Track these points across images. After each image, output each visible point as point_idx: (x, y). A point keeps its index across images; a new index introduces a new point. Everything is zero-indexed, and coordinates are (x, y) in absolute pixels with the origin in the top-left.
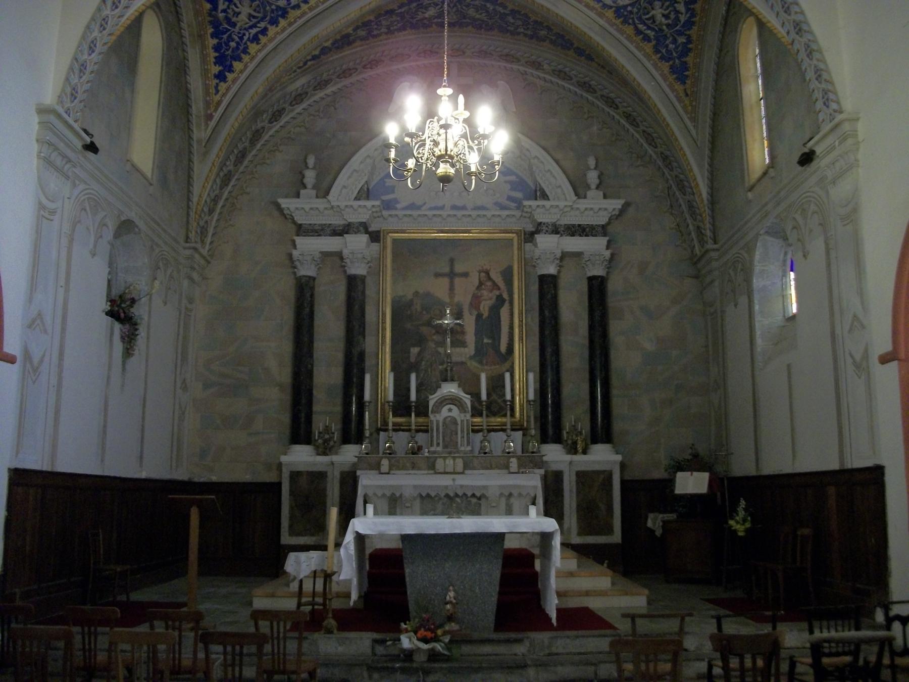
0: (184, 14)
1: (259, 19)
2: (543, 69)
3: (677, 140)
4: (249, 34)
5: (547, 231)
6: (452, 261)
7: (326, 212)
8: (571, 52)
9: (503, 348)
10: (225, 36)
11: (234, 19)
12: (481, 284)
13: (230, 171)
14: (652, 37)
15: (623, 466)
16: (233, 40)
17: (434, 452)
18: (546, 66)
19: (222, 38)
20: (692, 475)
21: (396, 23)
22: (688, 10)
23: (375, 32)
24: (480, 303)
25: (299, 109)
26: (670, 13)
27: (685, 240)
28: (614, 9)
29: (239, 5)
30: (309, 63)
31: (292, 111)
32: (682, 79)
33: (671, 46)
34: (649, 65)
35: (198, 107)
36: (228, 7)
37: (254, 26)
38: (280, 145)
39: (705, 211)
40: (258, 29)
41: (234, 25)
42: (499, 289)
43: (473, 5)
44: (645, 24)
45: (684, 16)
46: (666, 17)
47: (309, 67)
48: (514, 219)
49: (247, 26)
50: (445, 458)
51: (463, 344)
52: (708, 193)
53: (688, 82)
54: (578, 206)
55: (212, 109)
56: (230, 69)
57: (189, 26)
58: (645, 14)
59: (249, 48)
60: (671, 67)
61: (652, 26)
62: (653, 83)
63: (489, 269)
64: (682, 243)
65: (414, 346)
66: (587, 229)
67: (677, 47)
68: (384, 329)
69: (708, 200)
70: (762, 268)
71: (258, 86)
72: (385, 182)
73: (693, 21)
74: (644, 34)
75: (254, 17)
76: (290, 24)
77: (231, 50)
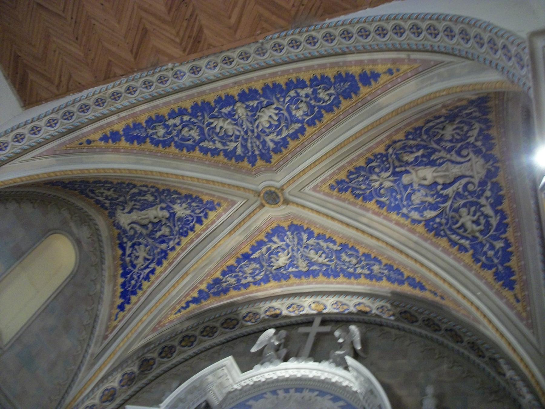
10: (129, 276)
11: (135, 262)
16: (133, 279)
22: (496, 212)
23: (244, 281)
26: (478, 219)
32: (510, 285)
35: (99, 329)
37: (147, 267)
41: (134, 266)
44: (458, 234)
46: (477, 222)
49: (143, 266)
53: (517, 287)
56: (128, 302)
60: (496, 274)
75: (148, 260)
76: (170, 264)
77: (131, 287)
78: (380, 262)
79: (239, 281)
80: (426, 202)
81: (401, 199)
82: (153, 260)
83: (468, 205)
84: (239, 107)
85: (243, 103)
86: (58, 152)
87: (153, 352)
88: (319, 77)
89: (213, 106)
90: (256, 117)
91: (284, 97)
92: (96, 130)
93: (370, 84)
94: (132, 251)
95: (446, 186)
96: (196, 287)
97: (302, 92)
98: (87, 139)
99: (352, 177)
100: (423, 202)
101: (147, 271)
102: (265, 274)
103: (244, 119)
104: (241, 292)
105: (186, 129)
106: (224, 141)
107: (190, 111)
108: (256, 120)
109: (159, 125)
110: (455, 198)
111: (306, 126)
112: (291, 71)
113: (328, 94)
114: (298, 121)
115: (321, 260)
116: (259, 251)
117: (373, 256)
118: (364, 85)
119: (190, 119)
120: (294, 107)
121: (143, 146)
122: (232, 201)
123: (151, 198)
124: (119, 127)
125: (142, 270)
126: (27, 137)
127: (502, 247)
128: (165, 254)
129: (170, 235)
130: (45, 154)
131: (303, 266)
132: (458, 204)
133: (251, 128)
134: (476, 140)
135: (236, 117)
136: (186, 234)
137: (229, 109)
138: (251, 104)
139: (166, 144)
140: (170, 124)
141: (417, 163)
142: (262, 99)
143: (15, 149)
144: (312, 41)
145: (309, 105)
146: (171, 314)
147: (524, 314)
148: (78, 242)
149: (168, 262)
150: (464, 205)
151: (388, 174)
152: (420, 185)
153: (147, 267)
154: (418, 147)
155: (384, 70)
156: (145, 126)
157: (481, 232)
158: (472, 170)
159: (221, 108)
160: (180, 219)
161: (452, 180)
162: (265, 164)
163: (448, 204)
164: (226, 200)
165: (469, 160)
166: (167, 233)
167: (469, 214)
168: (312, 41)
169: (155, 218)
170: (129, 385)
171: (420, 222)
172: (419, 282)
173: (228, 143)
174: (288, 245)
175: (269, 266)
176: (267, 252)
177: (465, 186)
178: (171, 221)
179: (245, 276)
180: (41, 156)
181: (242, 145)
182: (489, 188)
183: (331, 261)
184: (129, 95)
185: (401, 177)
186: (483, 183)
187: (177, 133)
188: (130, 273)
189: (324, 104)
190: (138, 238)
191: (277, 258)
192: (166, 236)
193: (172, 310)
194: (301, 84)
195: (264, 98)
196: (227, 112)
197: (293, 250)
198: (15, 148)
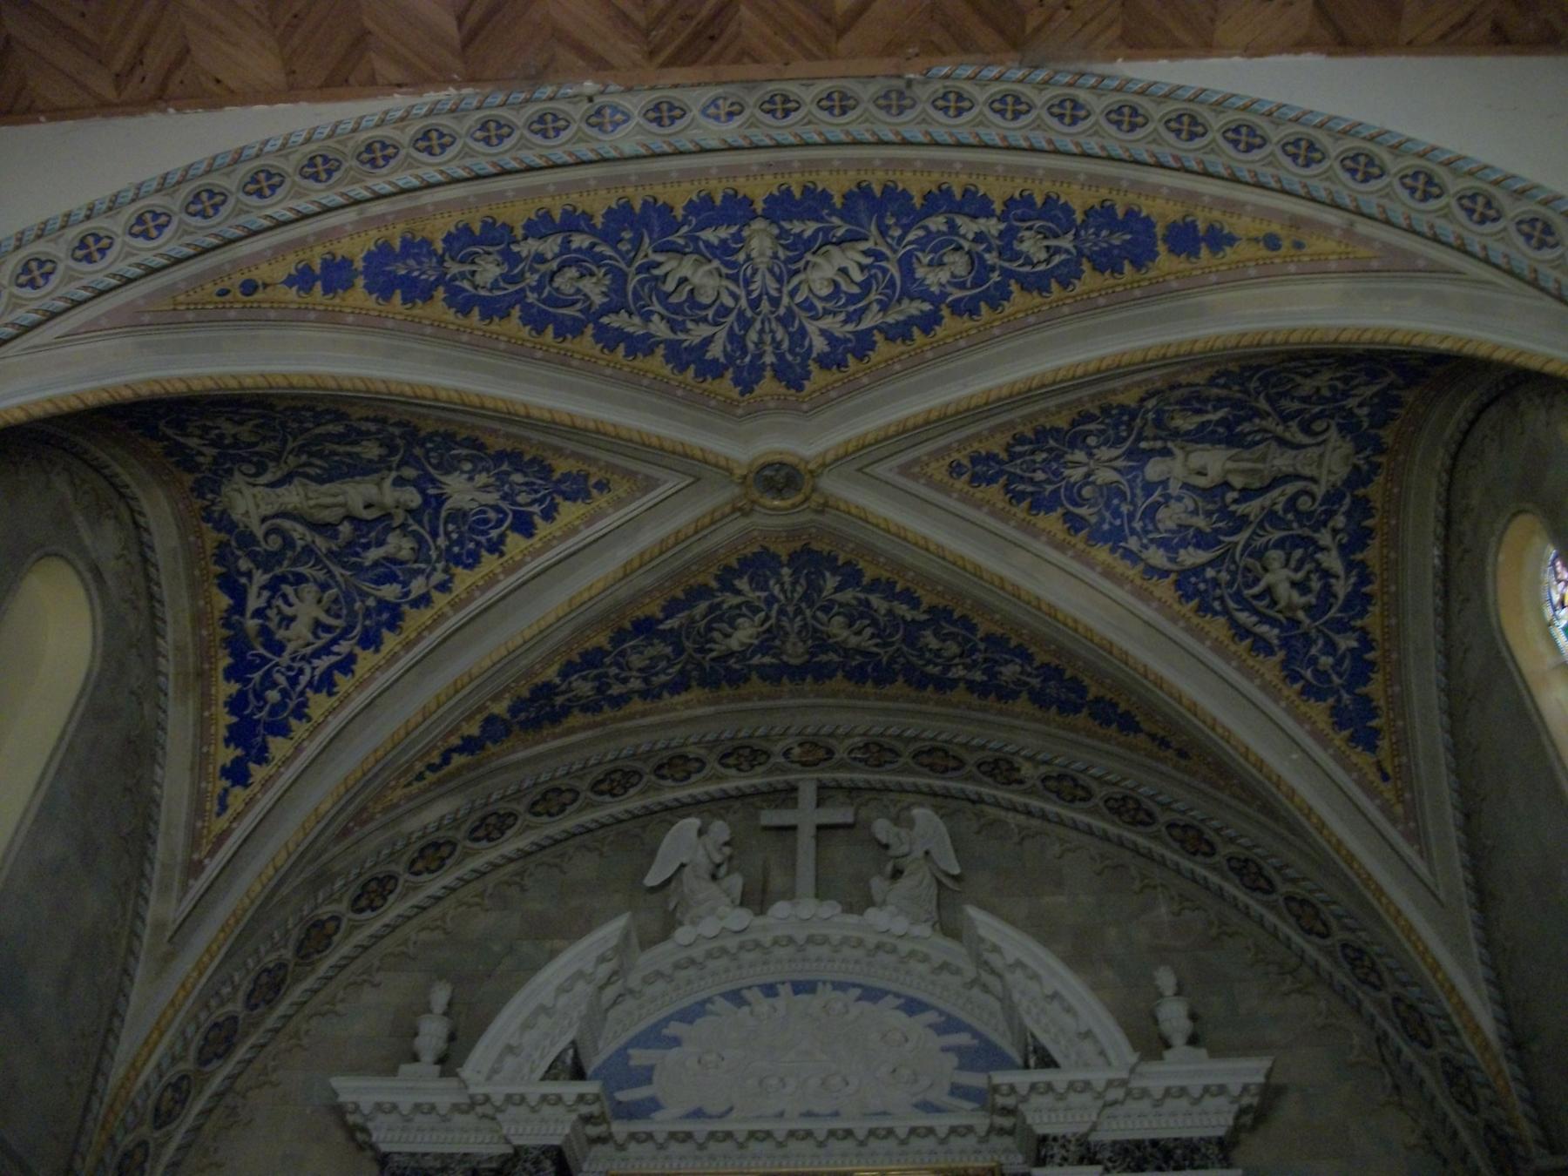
2: (1021, 782)
4: (314, 669)
7: (459, 1119)
8: (1082, 719)
10: (257, 676)
11: (281, 634)
13: (233, 1019)
14: (1276, 642)
16: (274, 685)
18: (1027, 770)
19: (250, 680)
21: (663, 664)
22: (1350, 565)
23: (616, 690)
25: (435, 885)
28: (1173, 577)
29: (292, 598)
30: (458, 760)
31: (416, 888)
32: (1367, 739)
33: (1326, 661)
35: (169, 843)
36: (269, 605)
37: (326, 650)
38: (379, 969)
39: (1500, 1072)
40: (333, 659)
41: (279, 648)
43: (841, 605)
44: (1255, 612)
45: (1342, 582)
46: (1301, 586)
47: (459, 770)
48: (971, 1141)
49: (309, 650)
52: (1497, 1020)
53: (1384, 743)
54: (1144, 1083)
55: (206, 848)
56: (262, 757)
57: (177, 648)
58: (1249, 586)
59: (311, 703)
61: (1271, 613)
62: (1294, 756)
66: (1179, 1152)
67: (1339, 662)
69: (1502, 1038)
71: (322, 794)
72: (629, 1057)
73: (1365, 595)
74: (1255, 635)
76: (409, 645)
77: (267, 708)
78: (1027, 657)
80: (1190, 526)
81: (1131, 516)
83: (1288, 544)
84: (757, 231)
85: (774, 222)
86: (146, 318)
87: (339, 901)
88: (1039, 200)
89: (680, 218)
90: (801, 264)
91: (907, 229)
92: (279, 251)
93: (1195, 253)
94: (269, 602)
95: (1247, 494)
96: (480, 709)
97: (968, 227)
98: (247, 276)
99: (1018, 449)
100: (1182, 527)
101: (323, 663)
103: (762, 267)
104: (599, 718)
105: (572, 272)
106: (680, 318)
107: (598, 221)
108: (797, 272)
109: (489, 253)
110: (1261, 525)
111: (945, 312)
112: (958, 166)
113: (1048, 248)
114: (925, 296)
116: (686, 613)
118: (1174, 250)
119: (593, 245)
120: (926, 260)
121: (419, 310)
122: (647, 477)
123: (371, 451)
124: (356, 248)
125: (306, 659)
126: (61, 267)
127: (1352, 650)
128: (393, 616)
130: (104, 322)
131: (795, 651)
132: (1264, 540)
133: (774, 293)
134: (1360, 405)
135: (741, 257)
137: (724, 233)
138: (797, 230)
139: (493, 309)
140: (524, 254)
141: (1201, 436)
142: (836, 220)
143: (20, 312)
144: (1070, 111)
145: (974, 259)
146: (394, 789)
147: (1399, 809)
150: (1279, 544)
151: (1115, 452)
152: (1186, 486)
153: (326, 650)
154: (1220, 402)
155: (1253, 234)
156: (440, 252)
157: (1308, 609)
158: (1320, 466)
159: (702, 227)
160: (458, 516)
161: (1267, 482)
162: (783, 390)
163: (1241, 538)
164: (630, 474)
165: (1324, 441)
166: (405, 554)
167: (1286, 564)
168: (1070, 111)
169: (368, 506)
170: (268, 1002)
171: (1165, 574)
173: (690, 325)
174: (771, 600)
176: (705, 617)
177: (1292, 503)
178: (426, 519)
179: (623, 675)
180: (89, 330)
181: (731, 335)
182: (1344, 509)
184: (424, 157)
185: (1145, 464)
186: (1334, 497)
187: (539, 281)
188: (258, 667)
189: (1027, 269)
190: (295, 562)
191: (730, 630)
192: (402, 563)
194: (977, 205)
195: (842, 218)
196: (716, 242)
197: (782, 612)
198: (21, 306)
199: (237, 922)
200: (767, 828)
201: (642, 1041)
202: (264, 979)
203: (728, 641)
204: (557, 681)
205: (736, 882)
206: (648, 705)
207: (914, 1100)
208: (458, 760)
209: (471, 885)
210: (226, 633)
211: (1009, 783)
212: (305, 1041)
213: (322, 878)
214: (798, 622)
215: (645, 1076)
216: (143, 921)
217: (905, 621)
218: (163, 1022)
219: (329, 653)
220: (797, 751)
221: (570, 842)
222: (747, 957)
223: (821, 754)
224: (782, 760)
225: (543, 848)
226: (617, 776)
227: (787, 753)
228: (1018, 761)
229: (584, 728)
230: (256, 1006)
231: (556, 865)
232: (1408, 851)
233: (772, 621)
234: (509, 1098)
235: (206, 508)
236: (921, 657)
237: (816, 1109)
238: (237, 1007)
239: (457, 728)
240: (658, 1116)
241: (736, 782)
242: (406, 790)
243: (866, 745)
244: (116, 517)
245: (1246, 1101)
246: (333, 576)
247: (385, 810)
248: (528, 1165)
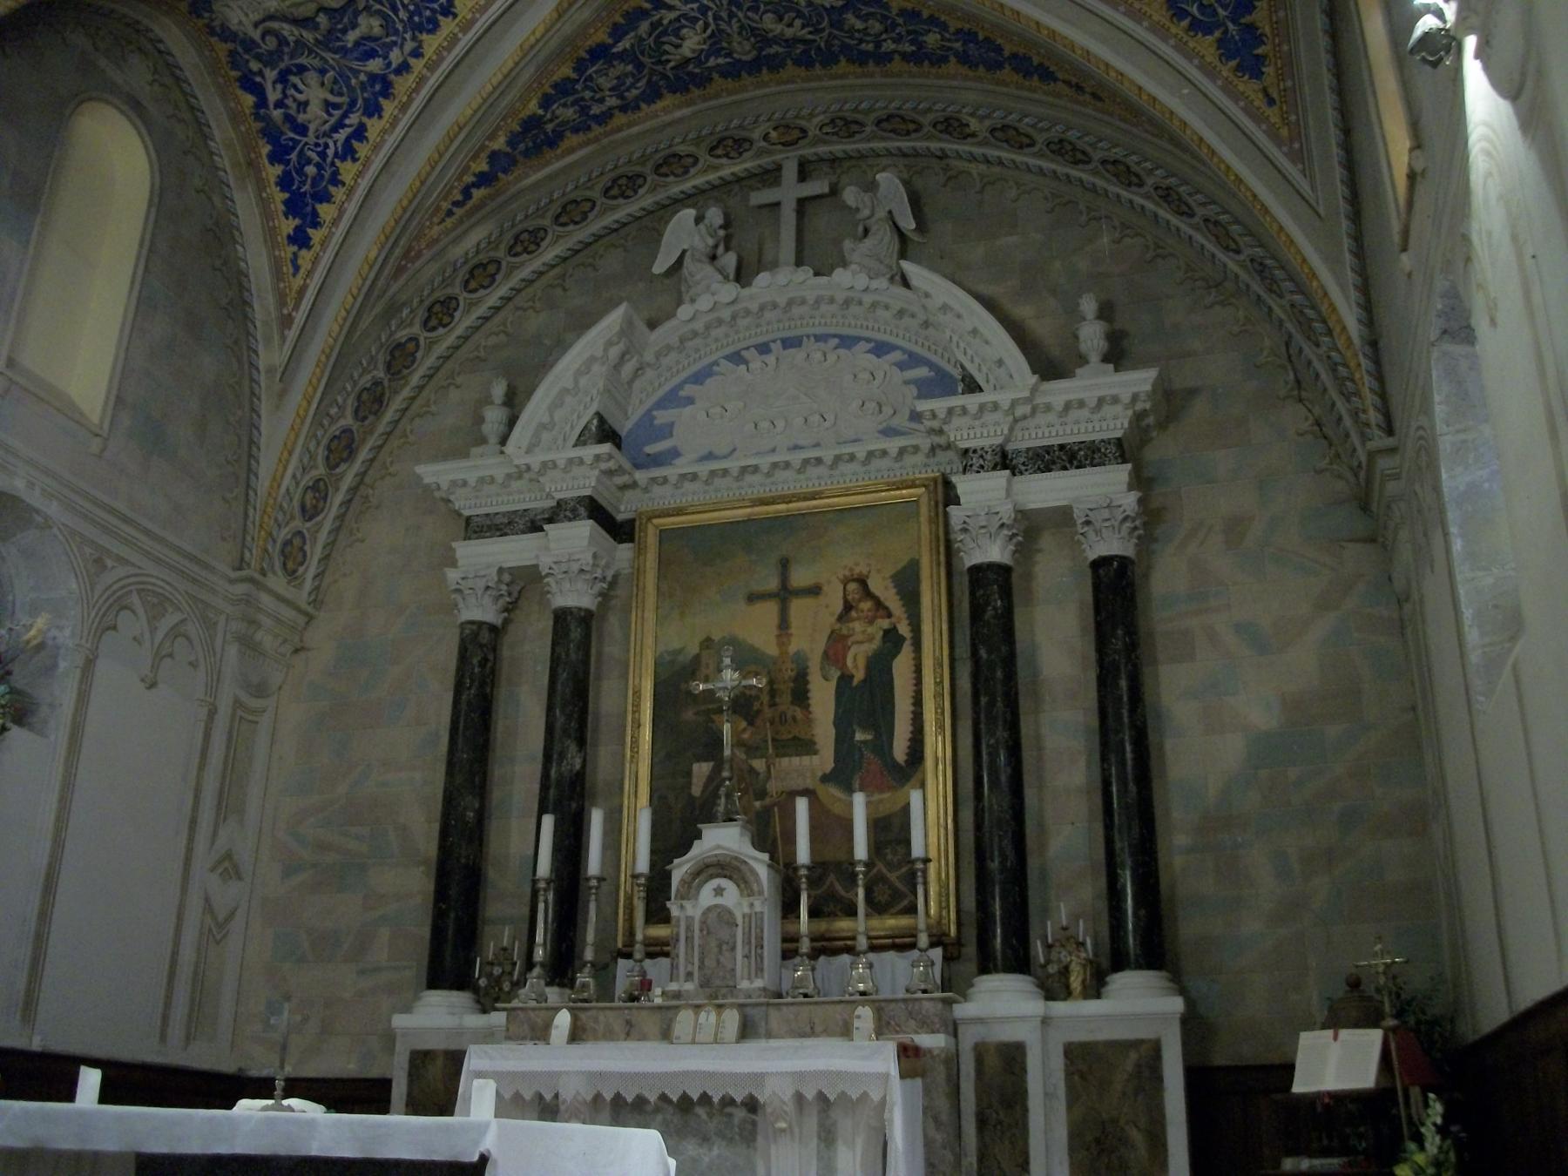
0: (213, 124)
1: (345, 107)
2: (973, 135)
3: (1266, 210)
4: (335, 143)
5: (982, 467)
6: (785, 564)
7: (516, 485)
8: (1006, 73)
9: (900, 751)
10: (294, 156)
11: (301, 118)
12: (848, 607)
13: (347, 431)
15: (1194, 1026)
16: (309, 161)
17: (677, 995)
18: (974, 125)
19: (289, 160)
20: (1335, 1038)
21: (629, 81)
23: (596, 110)
24: (847, 648)
27: (1338, 456)
29: (301, 86)
30: (478, 194)
32: (1252, 67)
34: (1165, 49)
35: (263, 306)
36: (285, 96)
40: (349, 130)
41: (302, 130)
42: (889, 615)
49: (327, 127)
50: (698, 1008)
51: (806, 746)
53: (1269, 70)
59: (341, 171)
60: (1221, 43)
62: (1186, 91)
63: (865, 572)
64: (1331, 464)
65: (700, 759)
68: (638, 725)
70: (1462, 436)
71: (367, 246)
72: (654, 418)
75: (336, 106)
76: (404, 108)
77: (309, 181)
78: (944, 27)
79: (584, 110)
82: (353, 103)
87: (411, 324)
94: (284, 92)
96: (483, 148)
101: (341, 135)
102: (649, 81)
104: (591, 135)
115: (789, 32)
116: (632, 34)
117: (925, 14)
125: (327, 135)
129: (387, 35)
131: (743, 49)
136: (434, 27)
146: (430, 228)
148: (135, 107)
149: (396, 102)
166: (377, 31)
172: (1041, 65)
175: (660, 62)
176: (650, 35)
179: (598, 96)
183: (817, 31)
188: (293, 148)
192: (376, 39)
193: (433, 215)
197: (717, 18)
199: (328, 357)
200: (761, 207)
201: (661, 404)
202: (365, 396)
203: (680, 51)
204: (541, 112)
205: (730, 260)
206: (631, 116)
207: (881, 427)
208: (478, 194)
209: (523, 293)
210: (260, 125)
211: (965, 138)
212: (412, 438)
213: (393, 309)
214: (735, 26)
215: (667, 431)
216: (257, 369)
217: (826, 9)
218: (289, 444)
219: (343, 126)
220: (774, 134)
221: (600, 242)
222: (742, 323)
223: (796, 134)
224: (763, 144)
225: (577, 252)
226: (623, 181)
227: (766, 137)
228: (966, 118)
229: (581, 146)
230: (365, 418)
231: (590, 265)
232: (1293, 171)
233: (713, 27)
234: (544, 464)
235: (208, 26)
236: (852, 38)
237: (801, 442)
238: (348, 420)
239: (467, 168)
240: (677, 462)
241: (730, 169)
242: (442, 226)
243: (832, 121)
244: (140, 49)
245: (1139, 406)
246: (326, 61)
247: (428, 246)
248: (568, 513)
